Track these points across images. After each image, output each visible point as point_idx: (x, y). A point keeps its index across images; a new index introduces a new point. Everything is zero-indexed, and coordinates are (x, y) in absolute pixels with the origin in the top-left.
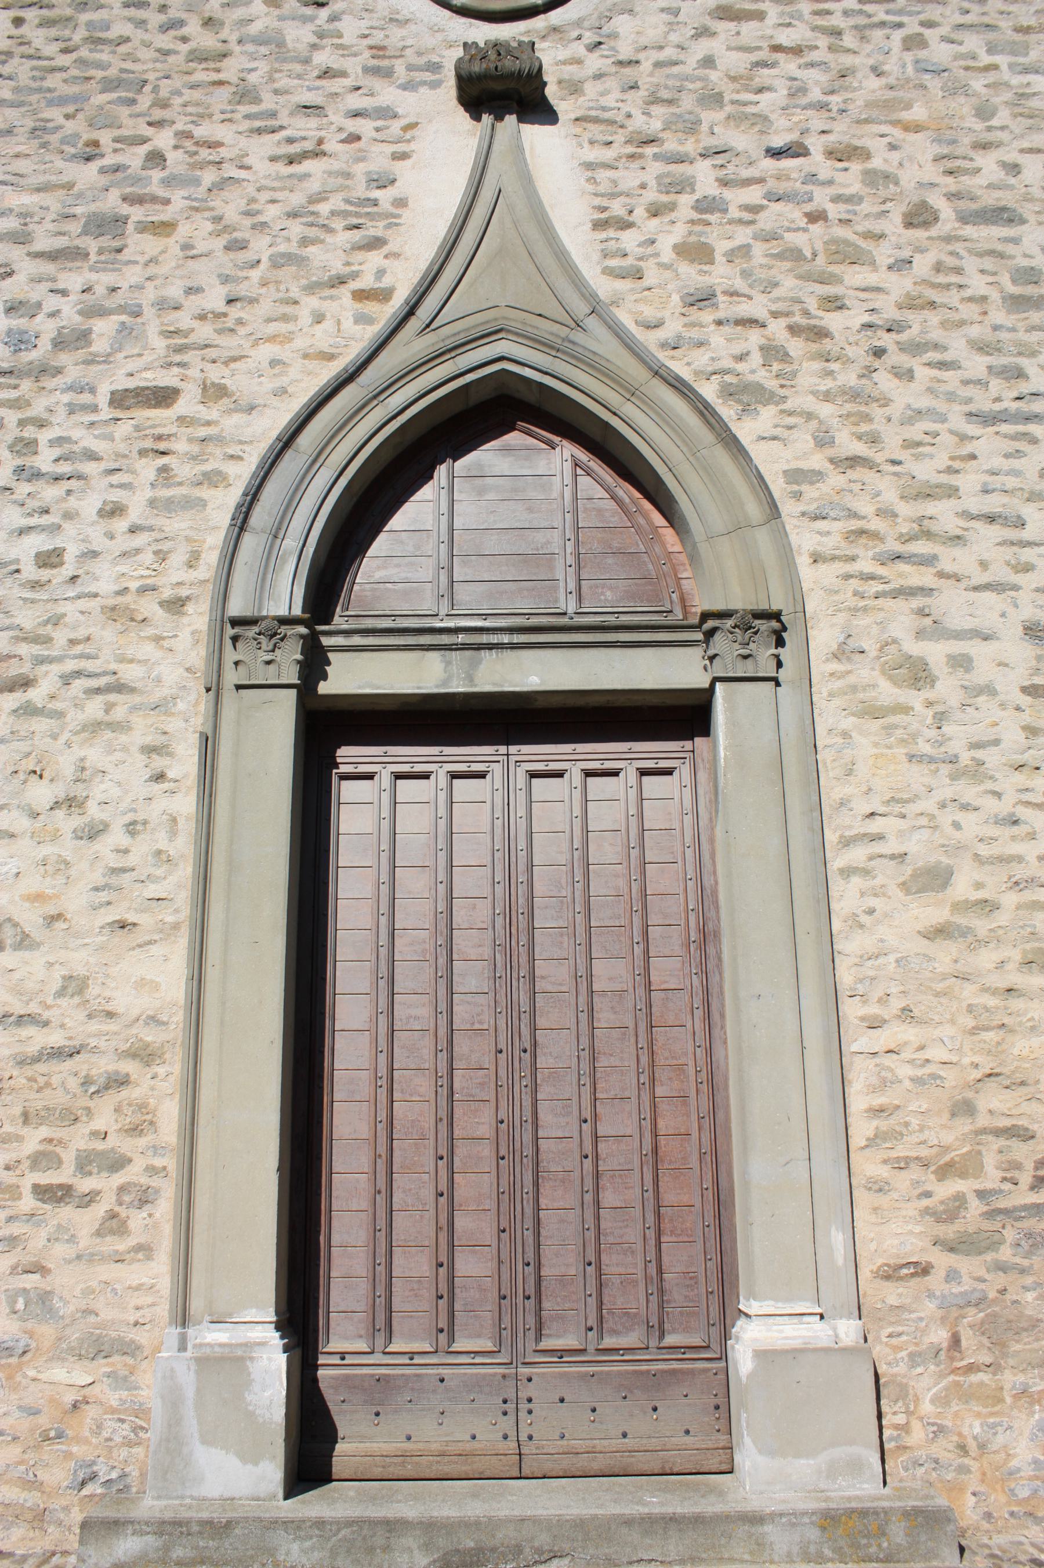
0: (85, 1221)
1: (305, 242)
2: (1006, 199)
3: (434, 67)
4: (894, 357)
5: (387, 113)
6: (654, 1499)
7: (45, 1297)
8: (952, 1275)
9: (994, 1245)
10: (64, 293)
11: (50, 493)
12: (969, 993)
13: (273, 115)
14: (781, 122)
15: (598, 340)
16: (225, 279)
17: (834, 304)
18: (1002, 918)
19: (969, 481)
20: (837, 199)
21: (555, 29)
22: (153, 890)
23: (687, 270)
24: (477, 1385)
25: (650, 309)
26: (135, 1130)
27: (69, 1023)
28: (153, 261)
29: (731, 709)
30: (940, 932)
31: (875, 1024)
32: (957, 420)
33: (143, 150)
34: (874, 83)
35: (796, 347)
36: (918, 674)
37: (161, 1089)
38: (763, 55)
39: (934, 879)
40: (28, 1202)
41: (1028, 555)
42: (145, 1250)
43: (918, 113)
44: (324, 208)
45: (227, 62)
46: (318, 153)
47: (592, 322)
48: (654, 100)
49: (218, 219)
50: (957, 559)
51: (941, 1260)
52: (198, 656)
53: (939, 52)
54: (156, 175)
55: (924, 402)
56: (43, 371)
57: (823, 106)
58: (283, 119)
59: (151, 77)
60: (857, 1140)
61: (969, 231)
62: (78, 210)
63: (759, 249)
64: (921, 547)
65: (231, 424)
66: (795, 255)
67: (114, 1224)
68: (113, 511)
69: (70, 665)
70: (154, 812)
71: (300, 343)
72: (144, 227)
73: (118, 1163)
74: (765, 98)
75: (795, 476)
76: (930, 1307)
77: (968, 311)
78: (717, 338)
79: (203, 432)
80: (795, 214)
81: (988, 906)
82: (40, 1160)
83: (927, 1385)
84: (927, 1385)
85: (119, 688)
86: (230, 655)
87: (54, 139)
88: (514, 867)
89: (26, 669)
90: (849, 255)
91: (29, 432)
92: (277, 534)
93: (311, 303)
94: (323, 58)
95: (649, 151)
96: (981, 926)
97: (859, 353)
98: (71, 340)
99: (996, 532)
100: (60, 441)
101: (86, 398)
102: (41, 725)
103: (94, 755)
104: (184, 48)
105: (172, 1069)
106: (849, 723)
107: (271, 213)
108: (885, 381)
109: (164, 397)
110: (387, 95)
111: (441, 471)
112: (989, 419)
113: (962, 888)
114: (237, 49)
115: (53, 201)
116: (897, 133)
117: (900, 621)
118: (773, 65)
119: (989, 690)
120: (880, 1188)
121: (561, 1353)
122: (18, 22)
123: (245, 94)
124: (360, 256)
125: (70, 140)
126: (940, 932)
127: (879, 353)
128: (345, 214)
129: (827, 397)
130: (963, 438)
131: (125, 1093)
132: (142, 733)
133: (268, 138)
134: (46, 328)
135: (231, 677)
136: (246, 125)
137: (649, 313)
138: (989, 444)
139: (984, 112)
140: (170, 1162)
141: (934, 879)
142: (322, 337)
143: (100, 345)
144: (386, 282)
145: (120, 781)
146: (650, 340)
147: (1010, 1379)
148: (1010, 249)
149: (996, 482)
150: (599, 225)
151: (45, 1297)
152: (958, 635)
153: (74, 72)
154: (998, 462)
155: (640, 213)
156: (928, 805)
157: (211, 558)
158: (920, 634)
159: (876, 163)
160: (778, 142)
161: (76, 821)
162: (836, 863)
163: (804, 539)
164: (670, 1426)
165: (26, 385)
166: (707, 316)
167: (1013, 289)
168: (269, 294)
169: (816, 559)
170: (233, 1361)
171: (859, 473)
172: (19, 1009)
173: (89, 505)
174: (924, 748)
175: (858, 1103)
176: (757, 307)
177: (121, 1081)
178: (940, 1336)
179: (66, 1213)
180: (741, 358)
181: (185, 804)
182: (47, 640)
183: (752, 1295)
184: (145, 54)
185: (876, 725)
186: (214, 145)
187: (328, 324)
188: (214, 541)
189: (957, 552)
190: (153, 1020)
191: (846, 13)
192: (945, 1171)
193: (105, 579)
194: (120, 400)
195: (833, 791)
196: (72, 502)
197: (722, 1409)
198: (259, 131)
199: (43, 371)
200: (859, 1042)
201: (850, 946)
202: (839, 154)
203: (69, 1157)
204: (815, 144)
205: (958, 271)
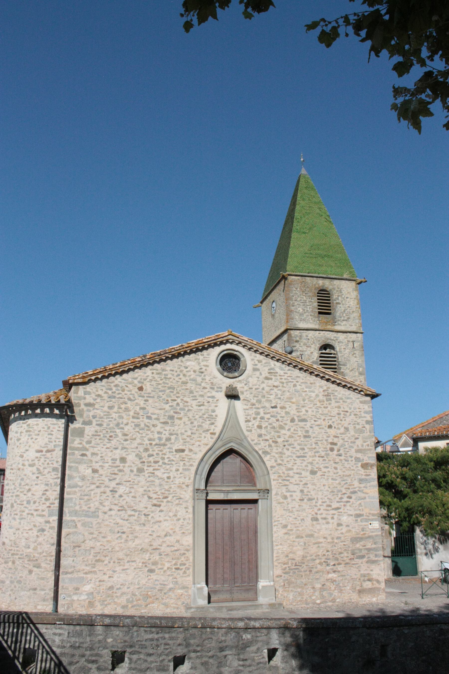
0: (181, 572)
1: (202, 423)
2: (305, 417)
3: (221, 388)
4: (287, 447)
5: (213, 397)
6: (250, 603)
7: (177, 582)
8: (284, 577)
9: (289, 573)
10: (166, 430)
11: (168, 467)
12: (289, 541)
13: (196, 396)
14: (274, 402)
15: (246, 444)
16: (191, 429)
17: (279, 437)
18: (294, 532)
19: (295, 467)
20: (281, 417)
21: (240, 381)
22: (187, 528)
23: (258, 430)
24: (227, 591)
25: (252, 437)
26: (187, 560)
27: (177, 546)
28: (179, 425)
29: (261, 503)
30: (286, 534)
31: (277, 545)
32: (295, 458)
33: (176, 402)
34: (288, 394)
35: (273, 444)
36: (285, 497)
37: (190, 555)
38: (271, 388)
39: (285, 526)
40: (174, 570)
41: (302, 479)
42: (189, 575)
43: (294, 400)
44: (205, 416)
45: (188, 384)
46: (203, 405)
47: (244, 440)
48: (255, 396)
49: (189, 417)
50: (292, 480)
51: (283, 575)
52: (191, 494)
53: (298, 388)
54: (178, 408)
55: (290, 454)
56: (164, 445)
57: (280, 398)
58: (198, 397)
59: (176, 387)
60: (274, 560)
61: (300, 423)
62: (167, 414)
63: (269, 426)
64: (288, 478)
65: (193, 456)
66: (274, 428)
67: (185, 572)
68: (177, 470)
69: (173, 495)
70: (187, 517)
71: (203, 442)
72: (177, 418)
73: (185, 564)
74: (272, 396)
75: (272, 467)
76: (282, 581)
77: (298, 438)
78: (262, 443)
79: (189, 457)
80: (274, 419)
81: (292, 530)
82: (175, 564)
83: (281, 590)
84: (281, 590)
85: (180, 498)
86: (196, 494)
87: (161, 399)
88: (232, 522)
89: (167, 495)
90: (281, 427)
91: (163, 456)
92: (201, 475)
93: (204, 434)
94: (203, 385)
95: (254, 407)
96: (291, 533)
97: (281, 446)
98: (168, 439)
99: (298, 475)
100: (168, 458)
101: (171, 450)
102: (170, 504)
103: (178, 508)
104: (181, 381)
105: (191, 552)
106: (276, 505)
107: (197, 417)
108: (285, 451)
109: (183, 451)
110: (214, 393)
111: (222, 462)
112: (298, 457)
113: (289, 528)
114: (189, 382)
115: (162, 412)
116: (290, 404)
117: (284, 489)
118: (273, 390)
119: (295, 500)
120: (276, 566)
121: (237, 586)
122: (153, 373)
123: (191, 392)
124: (210, 426)
125: (164, 399)
126: (286, 534)
127: (284, 446)
128: (208, 418)
129: (277, 453)
130: (295, 460)
131: (185, 556)
132: (184, 505)
133: (195, 401)
134: (164, 437)
135: (196, 498)
136: (192, 398)
137: (253, 438)
138: (298, 461)
139: (304, 400)
140: (192, 564)
141: (285, 526)
142: (205, 441)
143: (173, 441)
144: (215, 432)
145: (182, 513)
146: (252, 443)
147: (290, 589)
148: (305, 426)
149: (298, 467)
150: (246, 421)
151: (177, 582)
152: (291, 492)
153: (163, 385)
154: (299, 464)
155: (252, 419)
156: (285, 516)
157: (192, 479)
158: (287, 492)
159: (287, 410)
160: (273, 405)
161: (176, 518)
162: (274, 524)
163: (272, 477)
164: (250, 595)
165: (162, 447)
166: (261, 439)
167: (305, 434)
168: (197, 432)
169: (274, 480)
170: (201, 589)
171: (281, 466)
172: (170, 544)
173: (174, 469)
174: (286, 508)
175: (275, 555)
176: (267, 437)
177: (184, 554)
178: (283, 584)
179: (179, 571)
180: (265, 446)
181: (191, 516)
182: (170, 491)
183: (261, 579)
184: (174, 381)
185: (279, 505)
186: (187, 402)
187: (206, 438)
188: (193, 476)
189: (293, 479)
190: (188, 546)
191: (285, 379)
192: (284, 564)
193: (177, 481)
194: (177, 451)
195: (274, 514)
196: (171, 468)
197: (256, 593)
198: (193, 400)
199: (164, 445)
200: (275, 548)
201: (275, 535)
202: (282, 408)
203: (179, 564)
204: (278, 406)
205: (297, 431)
